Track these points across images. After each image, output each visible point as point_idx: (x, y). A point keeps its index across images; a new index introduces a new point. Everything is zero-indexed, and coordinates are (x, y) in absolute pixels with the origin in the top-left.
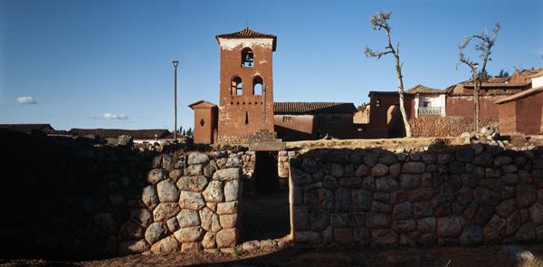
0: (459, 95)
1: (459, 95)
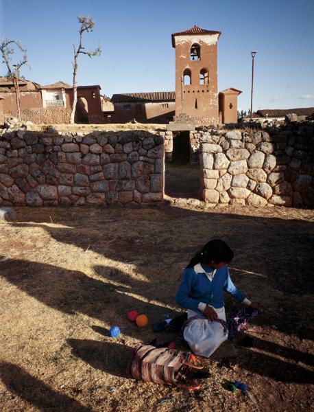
0: (31, 91)
1: (31, 91)
